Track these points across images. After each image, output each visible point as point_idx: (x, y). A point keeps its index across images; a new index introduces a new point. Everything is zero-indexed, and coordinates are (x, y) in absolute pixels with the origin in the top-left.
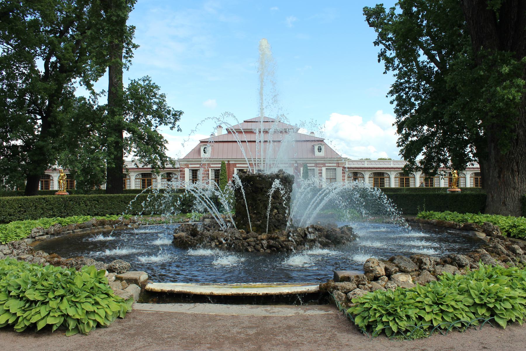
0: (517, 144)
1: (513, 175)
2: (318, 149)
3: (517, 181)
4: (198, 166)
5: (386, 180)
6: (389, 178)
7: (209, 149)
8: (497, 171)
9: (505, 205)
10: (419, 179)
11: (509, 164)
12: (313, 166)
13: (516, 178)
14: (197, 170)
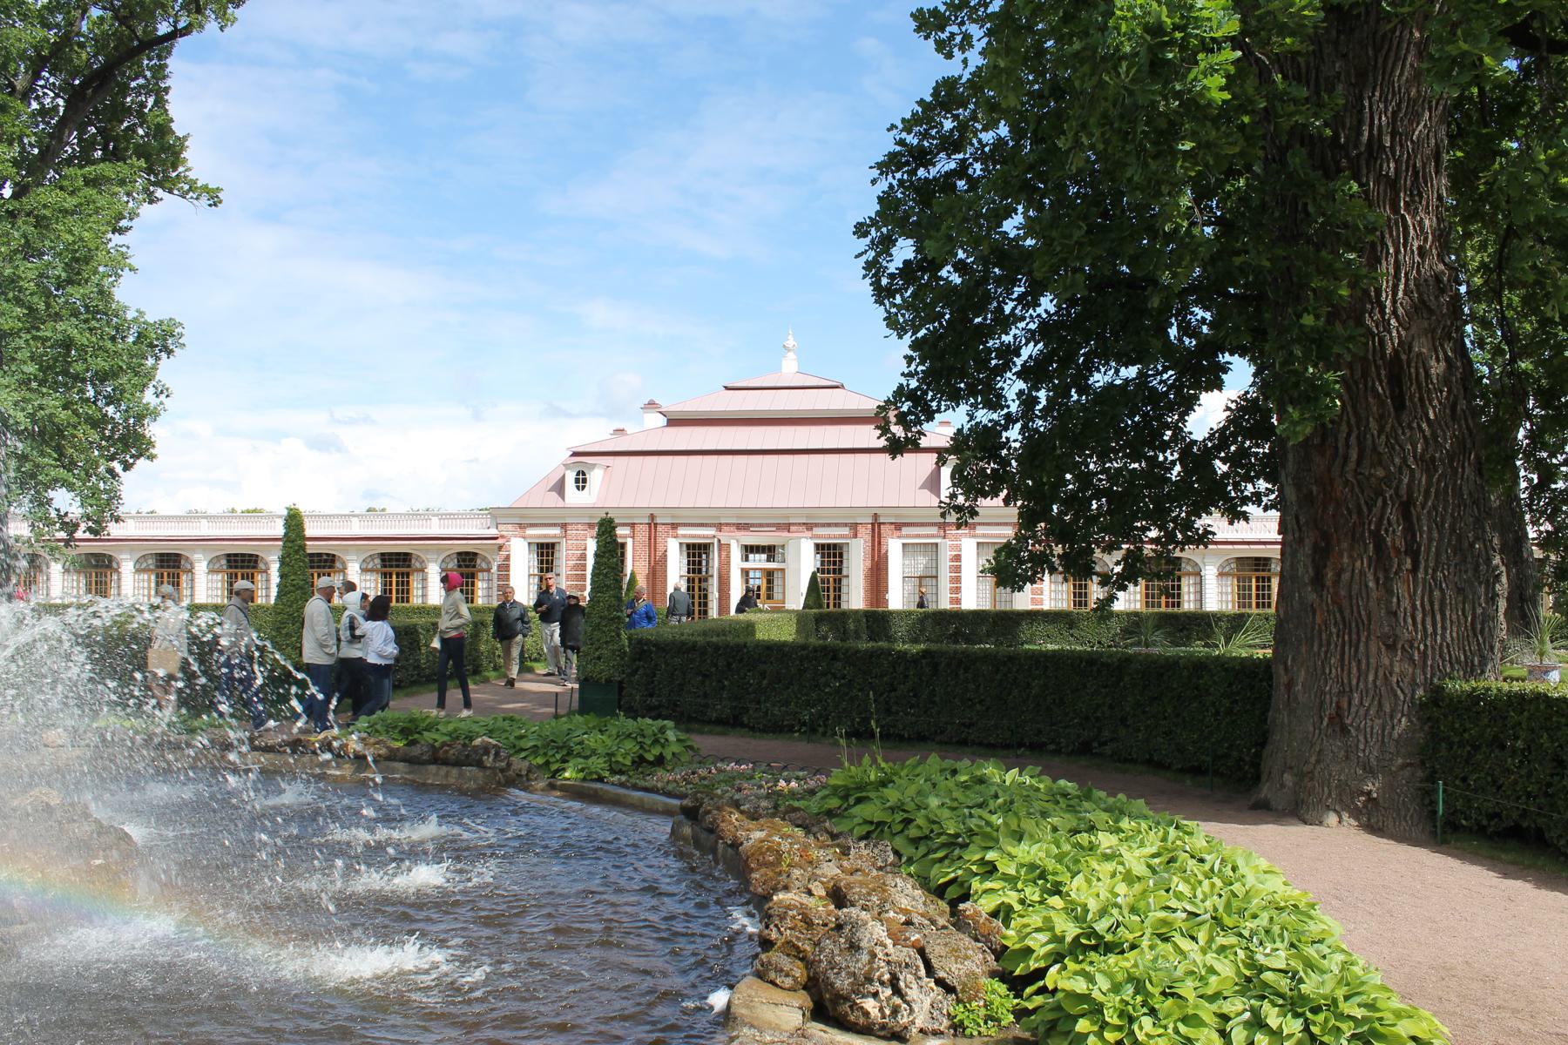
0: (1400, 406)
1: (1386, 571)
2: (577, 481)
3: (1406, 603)
4: (556, 531)
5: (415, 583)
6: (1198, 574)
7: (595, 477)
8: (1308, 549)
9: (1345, 730)
10: (1215, 582)
11: (1360, 512)
12: (932, 536)
13: (1400, 588)
14: (553, 545)
